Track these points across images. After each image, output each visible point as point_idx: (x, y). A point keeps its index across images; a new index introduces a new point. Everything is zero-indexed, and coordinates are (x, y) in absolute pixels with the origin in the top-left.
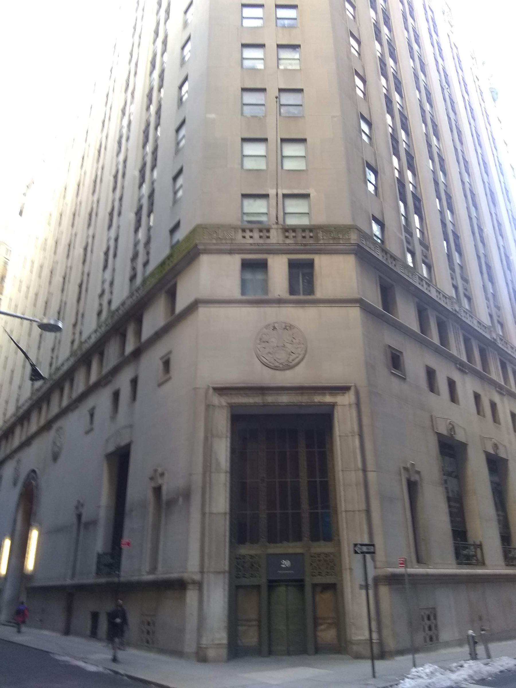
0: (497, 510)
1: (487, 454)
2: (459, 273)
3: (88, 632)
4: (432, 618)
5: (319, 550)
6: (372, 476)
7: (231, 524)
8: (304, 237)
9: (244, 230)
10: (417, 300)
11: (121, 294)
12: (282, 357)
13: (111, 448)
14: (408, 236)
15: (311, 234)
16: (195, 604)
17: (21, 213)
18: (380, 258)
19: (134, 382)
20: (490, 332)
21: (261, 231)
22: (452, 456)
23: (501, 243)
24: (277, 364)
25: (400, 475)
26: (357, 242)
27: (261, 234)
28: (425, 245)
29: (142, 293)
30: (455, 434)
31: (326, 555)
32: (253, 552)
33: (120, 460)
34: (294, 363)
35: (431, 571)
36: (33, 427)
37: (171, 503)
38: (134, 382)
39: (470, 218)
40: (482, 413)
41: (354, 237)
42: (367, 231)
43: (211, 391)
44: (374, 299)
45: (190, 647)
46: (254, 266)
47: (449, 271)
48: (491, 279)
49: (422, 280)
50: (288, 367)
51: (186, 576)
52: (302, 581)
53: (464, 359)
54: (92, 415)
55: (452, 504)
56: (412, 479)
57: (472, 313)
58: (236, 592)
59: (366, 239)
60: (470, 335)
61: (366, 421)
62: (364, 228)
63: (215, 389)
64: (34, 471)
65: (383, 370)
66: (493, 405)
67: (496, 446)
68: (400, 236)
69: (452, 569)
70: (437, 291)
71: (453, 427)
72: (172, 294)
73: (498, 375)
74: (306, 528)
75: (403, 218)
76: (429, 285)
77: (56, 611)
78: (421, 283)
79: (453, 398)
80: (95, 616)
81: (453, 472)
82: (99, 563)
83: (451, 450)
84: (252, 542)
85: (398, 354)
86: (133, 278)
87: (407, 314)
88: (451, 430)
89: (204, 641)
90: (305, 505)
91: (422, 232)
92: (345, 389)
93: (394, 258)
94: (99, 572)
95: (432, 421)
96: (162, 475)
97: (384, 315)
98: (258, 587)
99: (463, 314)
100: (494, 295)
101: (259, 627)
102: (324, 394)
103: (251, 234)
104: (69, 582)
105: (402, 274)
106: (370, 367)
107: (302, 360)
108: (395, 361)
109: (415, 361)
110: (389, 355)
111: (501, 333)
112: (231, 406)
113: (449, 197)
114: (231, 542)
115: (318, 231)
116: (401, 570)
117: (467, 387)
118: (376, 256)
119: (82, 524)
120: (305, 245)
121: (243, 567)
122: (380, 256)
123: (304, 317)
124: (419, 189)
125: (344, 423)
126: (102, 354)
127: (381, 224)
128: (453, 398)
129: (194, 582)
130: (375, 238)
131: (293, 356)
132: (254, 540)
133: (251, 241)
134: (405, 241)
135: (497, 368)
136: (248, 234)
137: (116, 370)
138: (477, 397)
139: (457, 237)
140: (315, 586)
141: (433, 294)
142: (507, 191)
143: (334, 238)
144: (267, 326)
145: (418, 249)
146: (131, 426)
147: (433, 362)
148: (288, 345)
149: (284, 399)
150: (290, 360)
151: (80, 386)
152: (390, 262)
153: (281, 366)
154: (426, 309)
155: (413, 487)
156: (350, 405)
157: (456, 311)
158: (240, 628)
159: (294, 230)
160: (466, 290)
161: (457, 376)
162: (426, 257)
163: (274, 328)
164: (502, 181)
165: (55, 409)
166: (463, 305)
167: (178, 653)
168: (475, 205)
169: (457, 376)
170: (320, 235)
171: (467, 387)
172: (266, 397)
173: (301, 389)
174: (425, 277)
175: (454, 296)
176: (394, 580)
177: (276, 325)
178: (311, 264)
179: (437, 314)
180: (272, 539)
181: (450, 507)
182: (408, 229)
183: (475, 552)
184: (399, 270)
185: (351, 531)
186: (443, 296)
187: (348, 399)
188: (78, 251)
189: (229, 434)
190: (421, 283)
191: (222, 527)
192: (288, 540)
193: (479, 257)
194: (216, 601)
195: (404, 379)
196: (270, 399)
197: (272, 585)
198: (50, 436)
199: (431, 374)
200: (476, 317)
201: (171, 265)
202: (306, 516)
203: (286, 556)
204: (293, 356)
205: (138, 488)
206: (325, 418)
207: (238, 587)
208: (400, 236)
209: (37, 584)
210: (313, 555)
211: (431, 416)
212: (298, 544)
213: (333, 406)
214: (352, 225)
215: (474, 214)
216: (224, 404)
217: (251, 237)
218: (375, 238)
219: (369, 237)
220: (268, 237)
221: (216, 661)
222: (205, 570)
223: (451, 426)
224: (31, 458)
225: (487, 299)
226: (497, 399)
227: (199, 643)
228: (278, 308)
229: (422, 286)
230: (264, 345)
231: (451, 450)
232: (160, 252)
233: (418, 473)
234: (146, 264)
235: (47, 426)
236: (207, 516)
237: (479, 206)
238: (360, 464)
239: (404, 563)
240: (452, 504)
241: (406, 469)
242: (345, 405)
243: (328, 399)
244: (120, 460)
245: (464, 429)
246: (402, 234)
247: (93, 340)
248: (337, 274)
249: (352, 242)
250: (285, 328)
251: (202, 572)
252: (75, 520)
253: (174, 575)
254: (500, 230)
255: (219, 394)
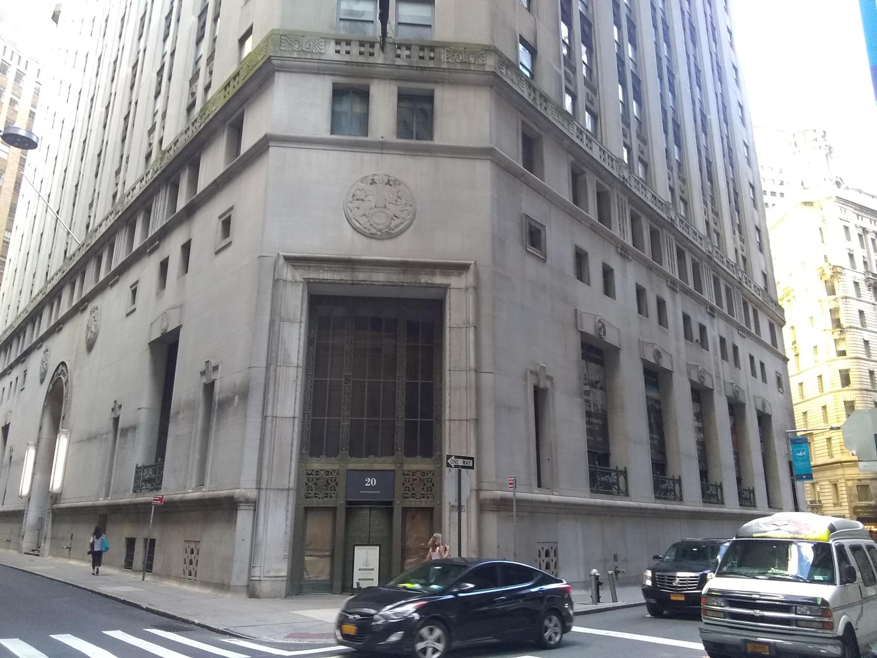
0: (651, 431)
1: (645, 362)
2: (636, 131)
3: (123, 563)
4: (552, 554)
5: (414, 467)
6: (487, 379)
7: (303, 431)
8: (422, 58)
9: (338, 42)
10: (573, 159)
11: (173, 130)
12: (381, 221)
13: (156, 335)
14: (569, 71)
15: (432, 55)
16: (249, 527)
17: (55, 17)
18: (526, 96)
19: (186, 248)
20: (668, 211)
21: (362, 44)
22: (601, 363)
23: (698, 96)
24: (374, 231)
25: (525, 378)
26: (493, 70)
27: (362, 49)
28: (592, 84)
29: (199, 126)
30: (605, 334)
31: (423, 473)
32: (328, 467)
33: (165, 350)
34: (397, 230)
35: (554, 498)
36: (64, 308)
37: (225, 404)
38: (186, 248)
39: (659, 58)
40: (644, 312)
41: (490, 63)
42: (512, 58)
43: (282, 261)
44: (512, 150)
45: (239, 578)
46: (350, 94)
47: (621, 125)
48: (678, 142)
49: (581, 132)
50: (389, 235)
51: (237, 493)
52: (391, 503)
53: (629, 242)
54: (134, 292)
55: (594, 420)
56: (541, 385)
57: (647, 182)
58: (304, 514)
59: (507, 67)
60: (639, 211)
61: (486, 309)
62: (508, 53)
63: (287, 259)
64: (63, 363)
65: (515, 248)
66: (661, 304)
67: (658, 354)
68: (558, 70)
69: (584, 497)
70: (600, 149)
71: (603, 326)
72: (237, 130)
73: (673, 267)
74: (400, 439)
75: (584, 66)
76: (590, 141)
77: (85, 536)
78: (580, 136)
79: (608, 289)
80: (131, 543)
81: (597, 382)
82: (137, 478)
83: (597, 353)
84: (328, 455)
85: (538, 227)
86: (190, 108)
87: (556, 176)
88: (600, 329)
89: (257, 572)
90: (401, 413)
91: (589, 69)
92: (462, 268)
93: (545, 99)
94: (137, 489)
95: (576, 317)
96: (216, 368)
97: (523, 175)
98: (334, 509)
99: (633, 183)
100: (680, 165)
101: (332, 557)
102: (433, 274)
103: (348, 48)
104: (102, 501)
105: (555, 123)
106: (498, 241)
107: (407, 227)
108: (534, 237)
109: (560, 241)
110: (526, 230)
111: (683, 214)
112: (309, 283)
113: (632, 26)
114: (301, 454)
115: (442, 50)
116: (509, 494)
117: (627, 278)
118: (520, 91)
119: (118, 429)
120: (423, 69)
121: (315, 484)
122: (525, 92)
123: (414, 171)
124: (590, 8)
125: (457, 312)
126: (148, 212)
127: (533, 52)
128: (608, 289)
129: (247, 501)
130: (521, 67)
131: (396, 221)
132: (333, 452)
133: (347, 58)
134: (563, 78)
135: (672, 257)
136: (344, 48)
137: (165, 232)
138: (640, 292)
139: (637, 81)
140: (405, 510)
141: (596, 153)
142: (714, 28)
143: (462, 63)
144: (363, 180)
145: (582, 92)
146: (181, 306)
147: (585, 242)
148: (389, 206)
149: (380, 277)
150: (392, 226)
151: (120, 254)
152: (538, 103)
153: (379, 233)
154: (584, 172)
155: (540, 396)
156: (467, 289)
157: (624, 178)
158: (307, 558)
159: (408, 48)
160: (642, 152)
161: (615, 263)
162: (591, 102)
163: (373, 182)
164: (708, 12)
165: (89, 285)
166: (636, 172)
167: (223, 586)
168: (667, 41)
169: (615, 263)
170: (444, 57)
171: (627, 278)
172: (357, 274)
173: (405, 266)
174: (587, 130)
175: (670, 201)
176: (502, 505)
177: (376, 178)
178: (429, 98)
179: (598, 179)
180: (355, 452)
181: (589, 423)
182: (569, 61)
183: (618, 480)
184: (551, 116)
185: (455, 440)
186: (609, 156)
187: (467, 280)
188: (125, 70)
189: (304, 319)
190: (580, 136)
191: (289, 434)
192: (376, 455)
193: (664, 112)
194: (276, 524)
195: (545, 261)
196: (361, 276)
197: (352, 508)
198: (83, 319)
199: (580, 257)
200: (652, 189)
201: (238, 87)
202: (400, 424)
203: (371, 473)
204: (396, 221)
205: (186, 385)
206: (436, 306)
207: (307, 509)
208: (558, 70)
209: (64, 504)
210: (406, 473)
211: (576, 310)
212: (390, 459)
213: (446, 288)
214: (489, 46)
215: (664, 52)
216: (299, 278)
217: (348, 53)
218: (521, 67)
219: (513, 66)
220: (372, 54)
221: (274, 596)
222: (263, 486)
223: (600, 325)
224: (63, 347)
225: (670, 168)
226: (667, 295)
227: (250, 576)
228: (380, 155)
229: (581, 140)
230: (357, 203)
231: (597, 353)
232: (225, 68)
233: (550, 378)
234: (207, 88)
235: (80, 308)
236: (269, 419)
237: (672, 44)
238: (472, 364)
239: (514, 484)
240: (594, 420)
241: (535, 373)
242: (460, 289)
243: (439, 280)
244: (165, 350)
245: (619, 330)
246: (560, 67)
247: (137, 192)
248: (466, 116)
249: (487, 69)
250: (388, 183)
251: (259, 489)
252: (110, 424)
253: (224, 493)
254: (698, 78)
255: (292, 266)
